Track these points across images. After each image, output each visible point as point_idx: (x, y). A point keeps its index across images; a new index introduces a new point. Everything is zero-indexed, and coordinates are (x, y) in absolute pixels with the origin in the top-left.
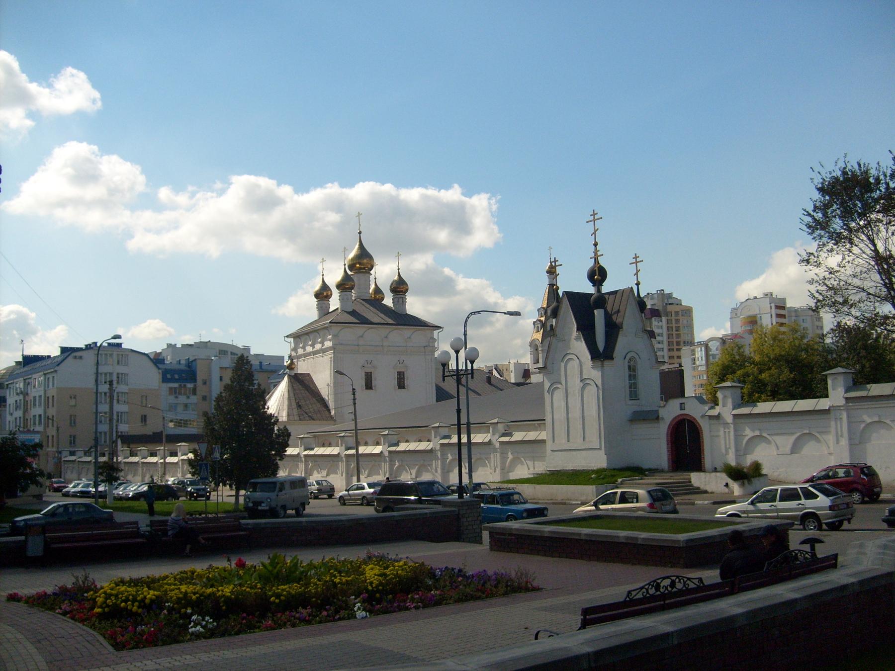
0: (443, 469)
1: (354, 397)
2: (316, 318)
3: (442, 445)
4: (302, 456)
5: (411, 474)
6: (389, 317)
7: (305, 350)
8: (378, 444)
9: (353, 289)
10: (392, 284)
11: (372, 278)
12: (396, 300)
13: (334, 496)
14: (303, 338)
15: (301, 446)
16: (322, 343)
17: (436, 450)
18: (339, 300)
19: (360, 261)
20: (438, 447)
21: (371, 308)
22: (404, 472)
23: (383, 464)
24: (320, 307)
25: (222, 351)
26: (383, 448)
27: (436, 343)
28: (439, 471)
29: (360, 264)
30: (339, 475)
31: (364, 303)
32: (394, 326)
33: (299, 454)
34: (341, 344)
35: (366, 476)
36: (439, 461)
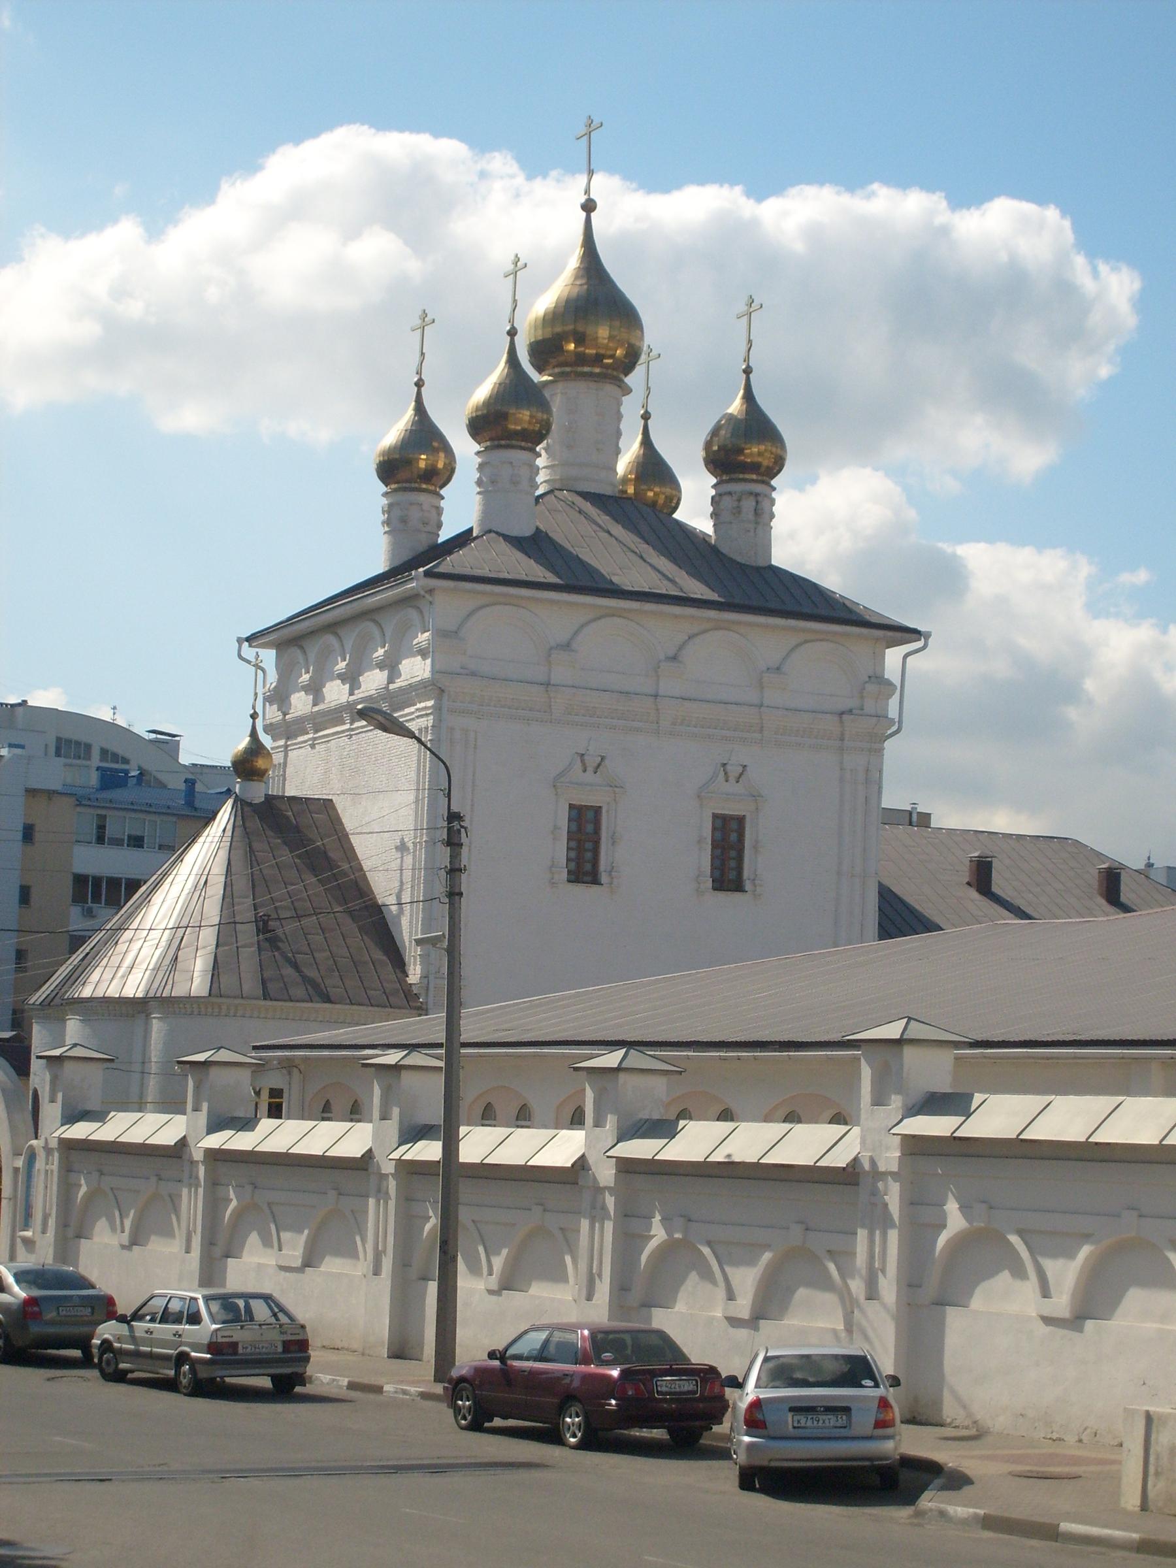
0: (911, 1283)
1: (455, 856)
2: (378, 565)
3: (916, 1146)
4: (198, 1156)
5: (731, 1296)
6: (696, 574)
7: (318, 698)
8: (355, 1113)
9: (539, 437)
10: (715, 432)
11: (631, 409)
12: (727, 502)
13: (301, 1379)
14: (314, 648)
15: (196, 1109)
16: (391, 665)
17: (877, 1175)
18: (479, 483)
19: (580, 328)
20: (890, 1158)
21: (618, 530)
22: (693, 1277)
23: (585, 1224)
24: (396, 522)
25: (68, 741)
26: (589, 1142)
27: (894, 703)
28: (888, 1288)
29: (580, 339)
30: (362, 1267)
31: (587, 506)
32: (712, 614)
33: (183, 1143)
34: (473, 674)
35: (493, 1282)
36: (893, 1236)
